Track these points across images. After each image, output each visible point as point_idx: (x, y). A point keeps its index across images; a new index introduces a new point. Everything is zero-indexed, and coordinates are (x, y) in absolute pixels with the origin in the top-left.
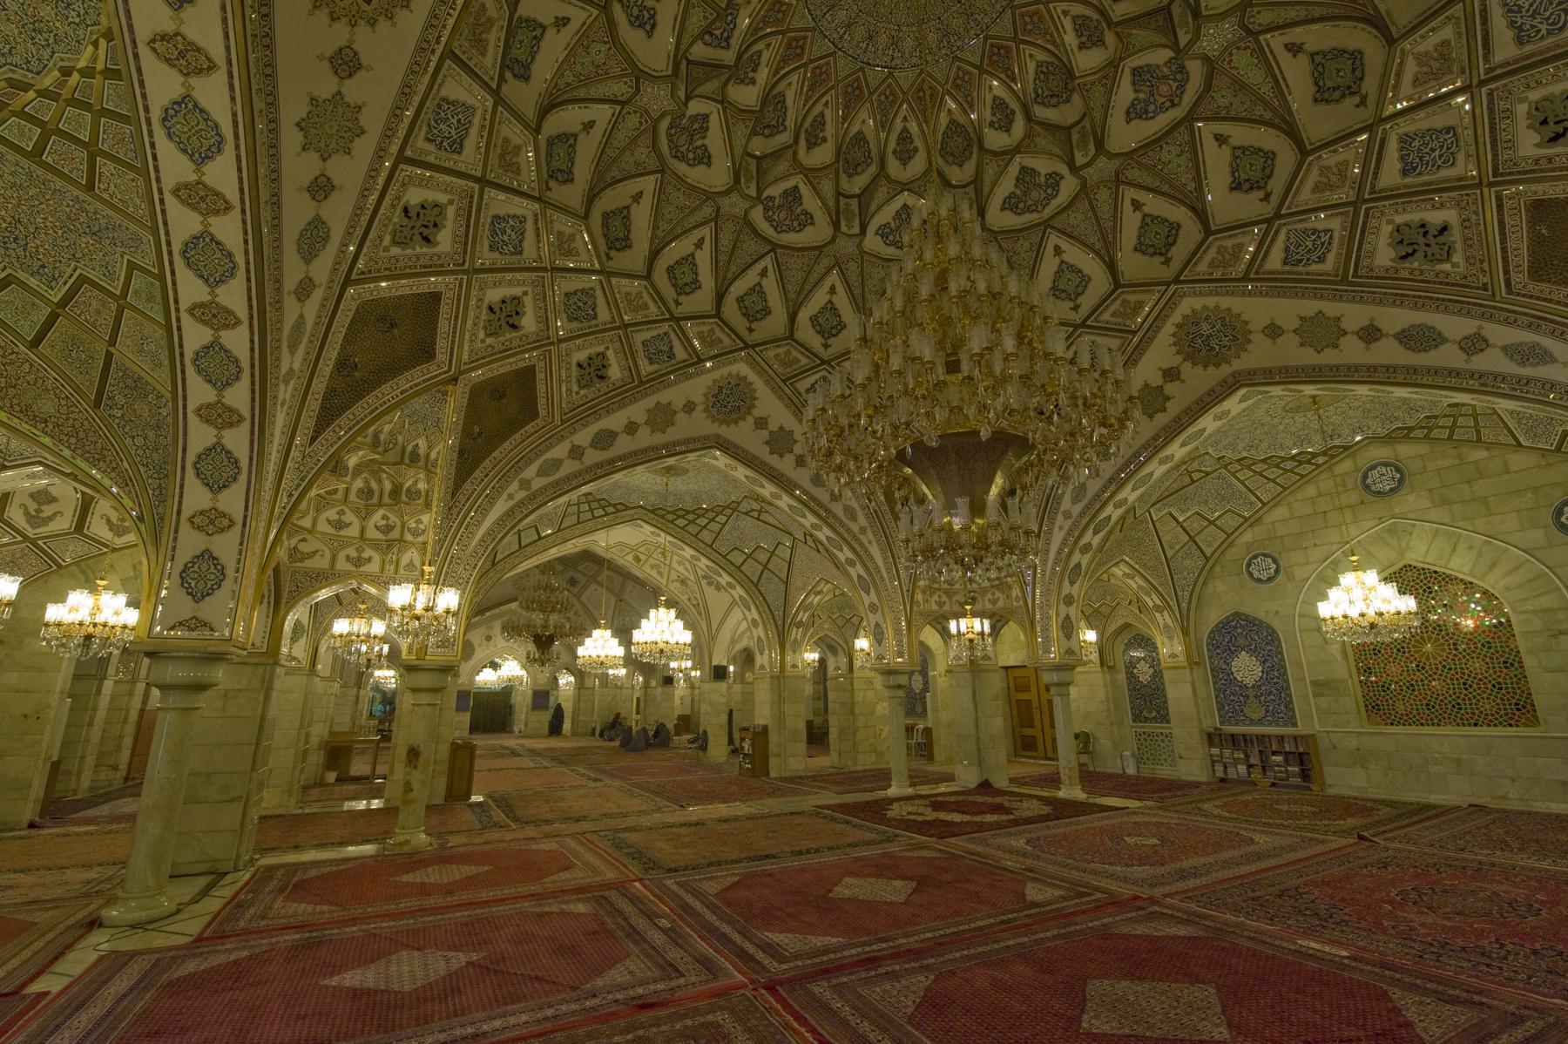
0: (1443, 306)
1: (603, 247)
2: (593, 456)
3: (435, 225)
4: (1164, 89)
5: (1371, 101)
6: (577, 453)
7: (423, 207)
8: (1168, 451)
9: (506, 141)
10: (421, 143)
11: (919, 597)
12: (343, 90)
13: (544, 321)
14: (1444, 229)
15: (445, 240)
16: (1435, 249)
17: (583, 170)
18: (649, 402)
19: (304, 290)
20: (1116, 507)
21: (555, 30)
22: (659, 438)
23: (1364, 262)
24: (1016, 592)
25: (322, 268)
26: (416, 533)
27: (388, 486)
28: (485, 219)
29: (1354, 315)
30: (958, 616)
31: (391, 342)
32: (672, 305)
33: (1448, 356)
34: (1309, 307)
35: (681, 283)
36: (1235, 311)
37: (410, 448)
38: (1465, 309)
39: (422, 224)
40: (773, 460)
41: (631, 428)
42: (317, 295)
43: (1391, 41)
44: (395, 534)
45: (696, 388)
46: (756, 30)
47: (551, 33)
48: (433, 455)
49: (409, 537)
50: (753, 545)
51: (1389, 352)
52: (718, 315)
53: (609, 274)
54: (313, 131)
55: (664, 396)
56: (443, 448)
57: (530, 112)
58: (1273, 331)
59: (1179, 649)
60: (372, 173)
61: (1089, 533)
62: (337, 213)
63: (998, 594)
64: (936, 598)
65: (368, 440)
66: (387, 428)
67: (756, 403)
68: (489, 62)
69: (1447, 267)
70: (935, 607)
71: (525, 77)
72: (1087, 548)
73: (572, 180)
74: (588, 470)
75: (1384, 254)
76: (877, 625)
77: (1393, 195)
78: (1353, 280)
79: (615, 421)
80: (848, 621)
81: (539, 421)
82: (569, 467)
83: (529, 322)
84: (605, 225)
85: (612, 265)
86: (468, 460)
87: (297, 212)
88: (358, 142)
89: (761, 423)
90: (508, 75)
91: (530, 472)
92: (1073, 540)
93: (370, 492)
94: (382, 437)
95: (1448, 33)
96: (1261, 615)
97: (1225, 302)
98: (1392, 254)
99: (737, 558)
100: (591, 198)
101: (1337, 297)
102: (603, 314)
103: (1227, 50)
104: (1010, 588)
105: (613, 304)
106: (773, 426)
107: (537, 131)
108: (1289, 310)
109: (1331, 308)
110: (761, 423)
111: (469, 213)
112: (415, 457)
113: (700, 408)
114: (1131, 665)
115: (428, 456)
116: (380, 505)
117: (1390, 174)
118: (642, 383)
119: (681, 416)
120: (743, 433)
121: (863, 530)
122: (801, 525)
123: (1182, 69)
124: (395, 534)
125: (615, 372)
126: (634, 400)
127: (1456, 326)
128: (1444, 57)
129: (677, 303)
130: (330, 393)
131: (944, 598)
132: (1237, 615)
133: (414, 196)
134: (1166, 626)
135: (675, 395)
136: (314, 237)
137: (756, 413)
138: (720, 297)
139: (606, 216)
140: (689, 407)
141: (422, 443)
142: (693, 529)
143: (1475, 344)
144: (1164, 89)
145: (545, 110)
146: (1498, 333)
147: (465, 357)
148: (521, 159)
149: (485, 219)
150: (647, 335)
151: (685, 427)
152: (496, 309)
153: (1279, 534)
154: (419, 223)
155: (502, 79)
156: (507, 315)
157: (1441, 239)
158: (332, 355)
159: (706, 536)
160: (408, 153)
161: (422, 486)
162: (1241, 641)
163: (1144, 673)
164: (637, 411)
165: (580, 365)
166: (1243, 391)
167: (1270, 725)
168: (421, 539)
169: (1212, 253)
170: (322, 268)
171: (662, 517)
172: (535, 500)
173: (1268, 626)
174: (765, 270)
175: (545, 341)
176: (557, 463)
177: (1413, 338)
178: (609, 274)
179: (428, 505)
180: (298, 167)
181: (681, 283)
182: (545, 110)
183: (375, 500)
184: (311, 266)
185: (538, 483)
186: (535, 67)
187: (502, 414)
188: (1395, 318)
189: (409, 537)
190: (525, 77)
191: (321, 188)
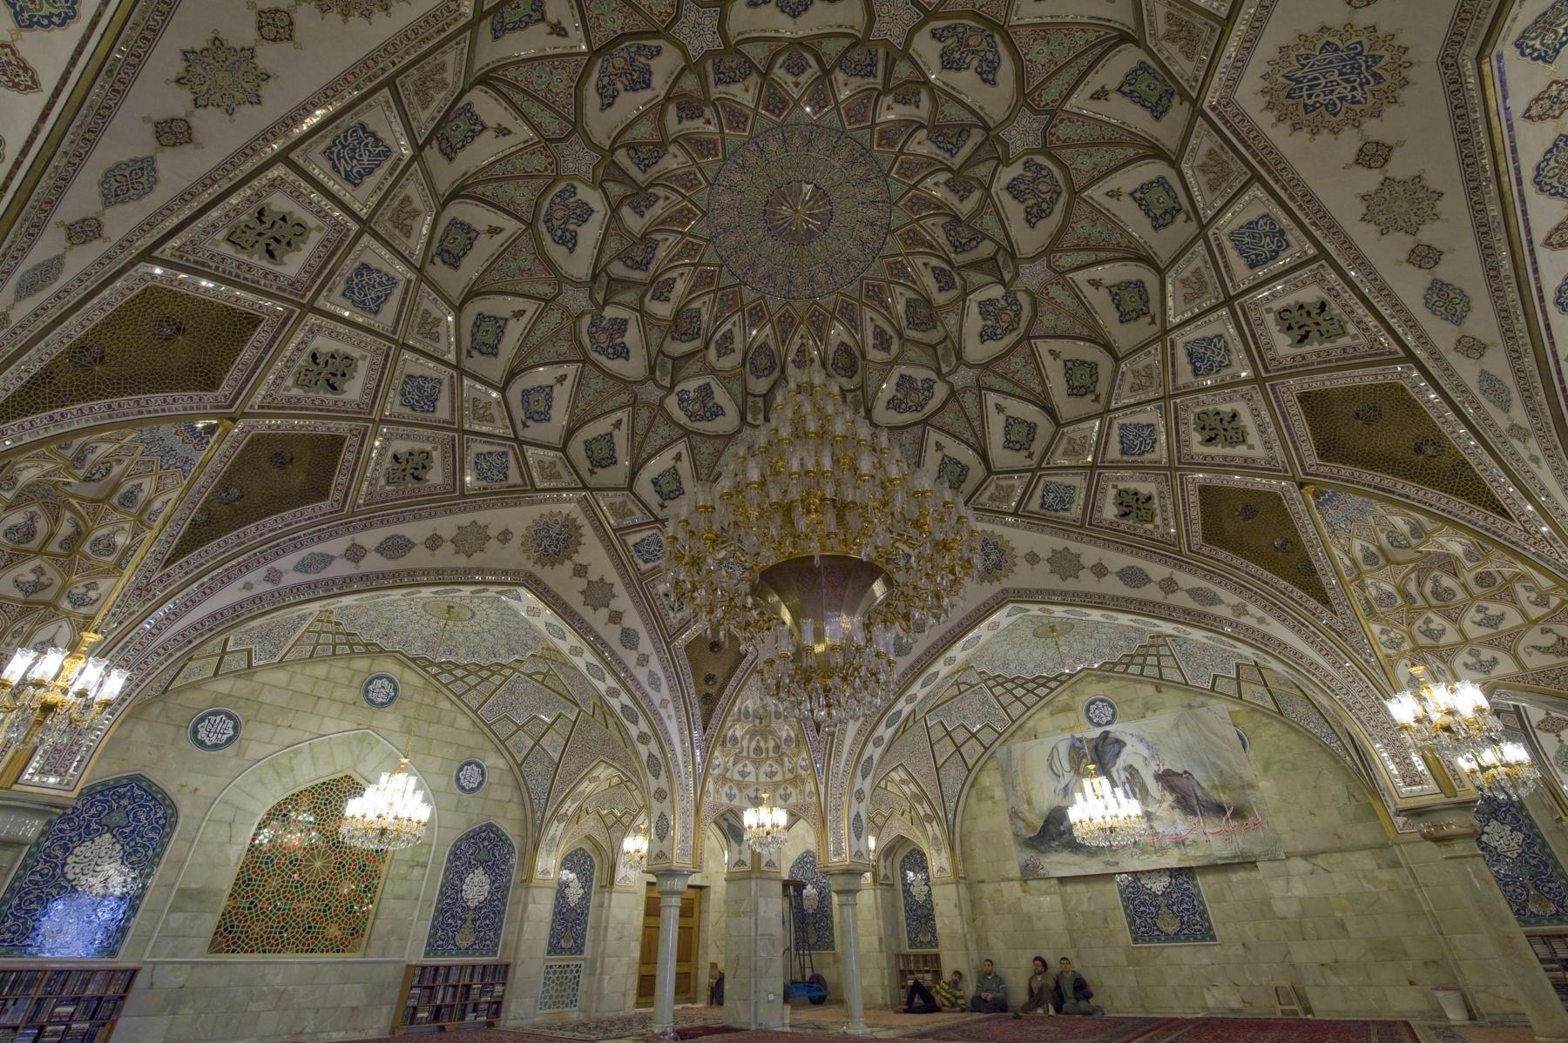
0: (1149, 555)
1: (467, 342)
2: (373, 563)
3: (289, 244)
4: (1005, 317)
5: (1103, 398)
6: (355, 554)
7: (284, 219)
8: (949, 654)
9: (407, 199)
10: (316, 153)
11: (710, 786)
12: (258, 50)
13: (375, 394)
14: (1149, 498)
15: (293, 264)
16: (1232, 433)
17: (472, 267)
18: (465, 519)
19: (84, 232)
20: (946, 664)
21: (548, 29)
22: (462, 561)
23: (1096, 515)
24: (810, 786)
25: (121, 221)
26: (79, 602)
27: (66, 529)
28: (349, 266)
29: (1090, 553)
30: (757, 802)
31: (172, 347)
32: (519, 426)
33: (1152, 593)
34: (1060, 543)
35: (532, 408)
36: (1006, 538)
37: (127, 486)
38: (1164, 560)
39: (274, 235)
40: (586, 613)
41: (434, 542)
42: (96, 249)
43: (1117, 360)
44: (47, 595)
45: (519, 518)
46: (663, 222)
47: (488, 135)
48: (157, 505)
49: (66, 605)
50: (526, 716)
51: (1112, 586)
52: (563, 449)
53: (463, 372)
54: (199, 69)
55: (482, 517)
56: (170, 500)
57: (444, 186)
58: (1033, 558)
59: (946, 865)
60: (247, 151)
61: (882, 727)
62: (177, 170)
63: (790, 789)
64: (726, 789)
65: (69, 453)
66: (104, 449)
67: (580, 549)
68: (425, 118)
69: (1150, 526)
70: (725, 800)
71: (449, 154)
72: (880, 740)
73: (457, 268)
74: (364, 577)
75: (1110, 511)
76: (662, 816)
77: (1115, 466)
78: (1088, 527)
79: (415, 530)
80: (618, 820)
81: (325, 505)
82: (341, 568)
83: (353, 390)
84: (477, 325)
85: (467, 364)
86: (197, 535)
87: (125, 139)
88: (245, 110)
89: (581, 571)
90: (435, 143)
91: (286, 563)
92: (866, 736)
93: (30, 533)
94: (91, 458)
95: (1150, 360)
96: (171, 788)
97: (999, 530)
98: (1115, 511)
99: (505, 730)
100: (472, 294)
101: (1079, 538)
102: (443, 411)
103: (965, 389)
104: (803, 782)
105: (456, 405)
106: (593, 575)
107: (444, 205)
108: (1045, 543)
109: (1075, 547)
110: (581, 571)
111: (338, 246)
112: (129, 499)
113: (516, 541)
114: (907, 886)
115: (149, 502)
116: (40, 552)
117: (1114, 451)
118: (463, 495)
119: (493, 543)
120: (558, 576)
121: (664, 704)
122: (594, 688)
123: (1016, 302)
124: (47, 595)
125: (435, 476)
126: (448, 512)
127: (1157, 571)
128: (1149, 376)
129: (525, 425)
130: (46, 376)
131: (735, 791)
132: (137, 780)
133: (279, 203)
134: (935, 838)
135: (495, 519)
136: (129, 181)
137: (578, 559)
138: (570, 433)
139: (481, 317)
140: (505, 536)
141: (148, 484)
142: (459, 687)
143: (1169, 586)
144: (1005, 317)
145: (457, 194)
146: (1187, 580)
147: (257, 399)
148: (416, 224)
149: (349, 266)
150: (486, 449)
151: (494, 554)
152: (321, 360)
153: (262, 699)
154: (270, 234)
155: (428, 141)
156: (332, 372)
157: (1233, 425)
158: (74, 328)
159: (473, 699)
160: (293, 156)
161: (121, 540)
162: (117, 818)
163: (918, 892)
164: (447, 525)
165: (396, 458)
166: (1010, 606)
167: (473, 955)
168: (83, 610)
169: (992, 489)
170: (121, 221)
171: (424, 668)
172: (280, 599)
173: (173, 806)
174: (619, 422)
175: (366, 416)
176: (327, 560)
177: (1134, 577)
178: (463, 372)
179: (119, 567)
180: (156, 92)
181: (532, 408)
182: (457, 194)
183: (34, 545)
184: (109, 211)
185: (292, 579)
186: (461, 155)
187: (284, 479)
188: (1118, 560)
189: (66, 605)
190: (449, 154)
191: (173, 133)
